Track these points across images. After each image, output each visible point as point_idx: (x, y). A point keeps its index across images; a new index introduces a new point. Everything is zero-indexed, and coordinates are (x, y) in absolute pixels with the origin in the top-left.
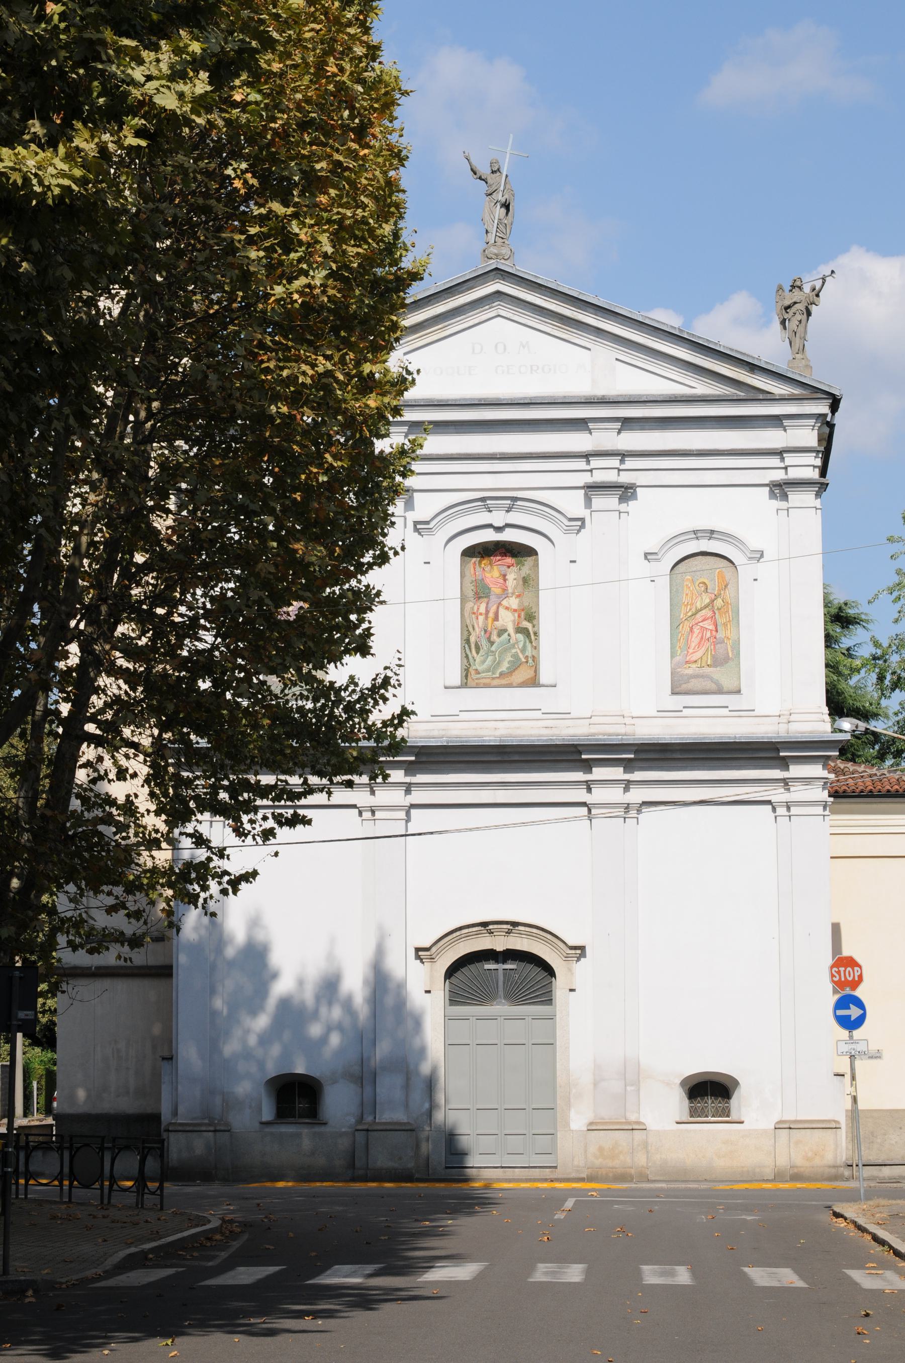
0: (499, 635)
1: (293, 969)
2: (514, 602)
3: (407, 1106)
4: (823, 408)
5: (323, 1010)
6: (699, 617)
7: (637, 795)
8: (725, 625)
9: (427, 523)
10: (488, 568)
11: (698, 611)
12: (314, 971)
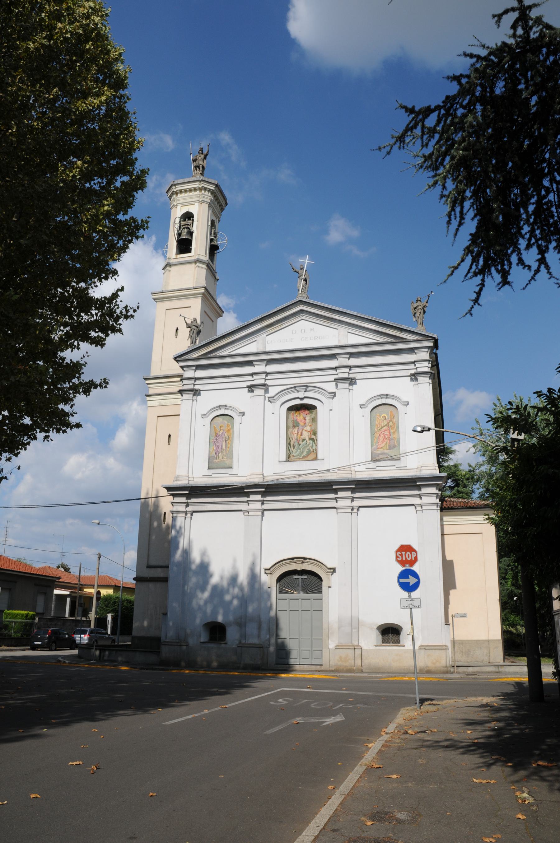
0: (303, 441)
1: (219, 572)
2: (308, 428)
3: (259, 636)
4: (431, 344)
5: (231, 590)
6: (383, 430)
7: (356, 503)
8: (394, 432)
9: (273, 397)
10: (298, 415)
11: (382, 428)
12: (227, 574)
